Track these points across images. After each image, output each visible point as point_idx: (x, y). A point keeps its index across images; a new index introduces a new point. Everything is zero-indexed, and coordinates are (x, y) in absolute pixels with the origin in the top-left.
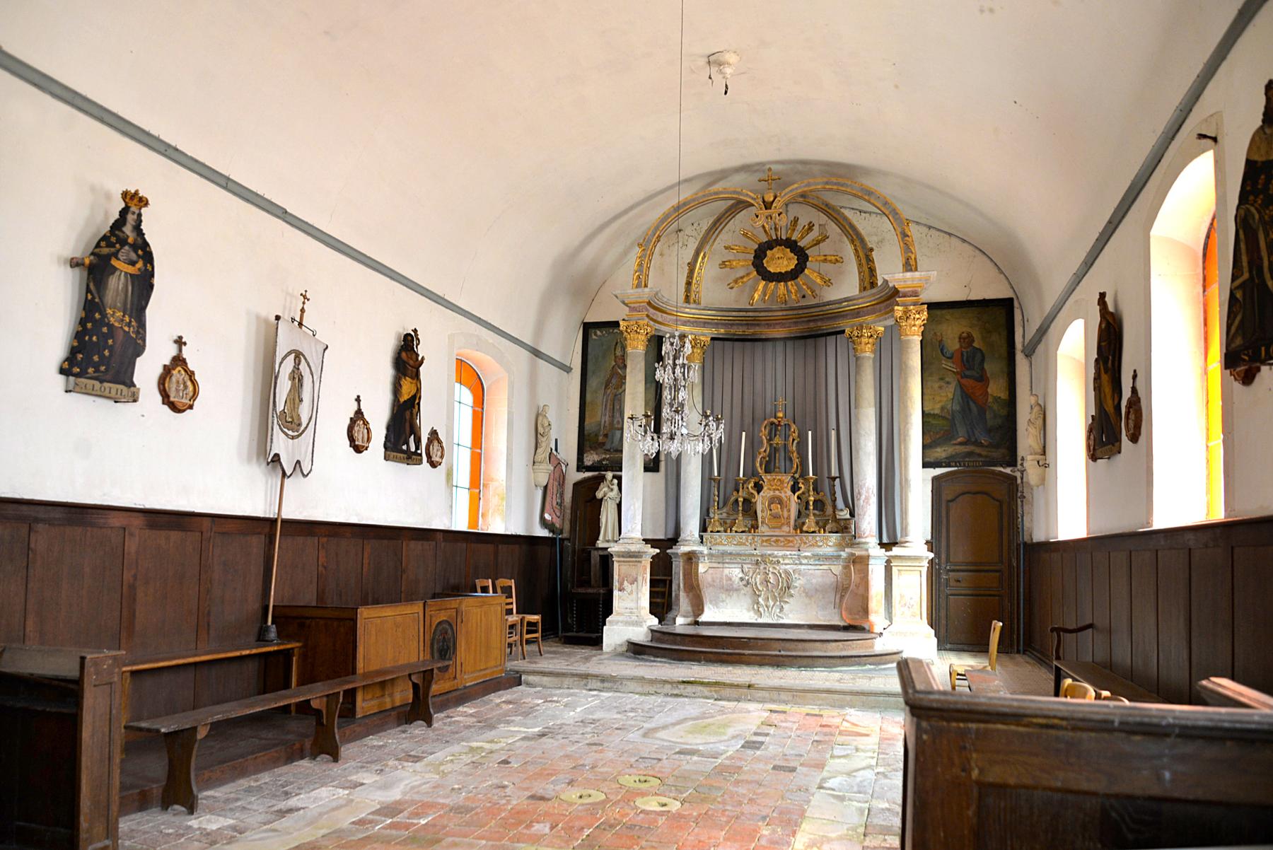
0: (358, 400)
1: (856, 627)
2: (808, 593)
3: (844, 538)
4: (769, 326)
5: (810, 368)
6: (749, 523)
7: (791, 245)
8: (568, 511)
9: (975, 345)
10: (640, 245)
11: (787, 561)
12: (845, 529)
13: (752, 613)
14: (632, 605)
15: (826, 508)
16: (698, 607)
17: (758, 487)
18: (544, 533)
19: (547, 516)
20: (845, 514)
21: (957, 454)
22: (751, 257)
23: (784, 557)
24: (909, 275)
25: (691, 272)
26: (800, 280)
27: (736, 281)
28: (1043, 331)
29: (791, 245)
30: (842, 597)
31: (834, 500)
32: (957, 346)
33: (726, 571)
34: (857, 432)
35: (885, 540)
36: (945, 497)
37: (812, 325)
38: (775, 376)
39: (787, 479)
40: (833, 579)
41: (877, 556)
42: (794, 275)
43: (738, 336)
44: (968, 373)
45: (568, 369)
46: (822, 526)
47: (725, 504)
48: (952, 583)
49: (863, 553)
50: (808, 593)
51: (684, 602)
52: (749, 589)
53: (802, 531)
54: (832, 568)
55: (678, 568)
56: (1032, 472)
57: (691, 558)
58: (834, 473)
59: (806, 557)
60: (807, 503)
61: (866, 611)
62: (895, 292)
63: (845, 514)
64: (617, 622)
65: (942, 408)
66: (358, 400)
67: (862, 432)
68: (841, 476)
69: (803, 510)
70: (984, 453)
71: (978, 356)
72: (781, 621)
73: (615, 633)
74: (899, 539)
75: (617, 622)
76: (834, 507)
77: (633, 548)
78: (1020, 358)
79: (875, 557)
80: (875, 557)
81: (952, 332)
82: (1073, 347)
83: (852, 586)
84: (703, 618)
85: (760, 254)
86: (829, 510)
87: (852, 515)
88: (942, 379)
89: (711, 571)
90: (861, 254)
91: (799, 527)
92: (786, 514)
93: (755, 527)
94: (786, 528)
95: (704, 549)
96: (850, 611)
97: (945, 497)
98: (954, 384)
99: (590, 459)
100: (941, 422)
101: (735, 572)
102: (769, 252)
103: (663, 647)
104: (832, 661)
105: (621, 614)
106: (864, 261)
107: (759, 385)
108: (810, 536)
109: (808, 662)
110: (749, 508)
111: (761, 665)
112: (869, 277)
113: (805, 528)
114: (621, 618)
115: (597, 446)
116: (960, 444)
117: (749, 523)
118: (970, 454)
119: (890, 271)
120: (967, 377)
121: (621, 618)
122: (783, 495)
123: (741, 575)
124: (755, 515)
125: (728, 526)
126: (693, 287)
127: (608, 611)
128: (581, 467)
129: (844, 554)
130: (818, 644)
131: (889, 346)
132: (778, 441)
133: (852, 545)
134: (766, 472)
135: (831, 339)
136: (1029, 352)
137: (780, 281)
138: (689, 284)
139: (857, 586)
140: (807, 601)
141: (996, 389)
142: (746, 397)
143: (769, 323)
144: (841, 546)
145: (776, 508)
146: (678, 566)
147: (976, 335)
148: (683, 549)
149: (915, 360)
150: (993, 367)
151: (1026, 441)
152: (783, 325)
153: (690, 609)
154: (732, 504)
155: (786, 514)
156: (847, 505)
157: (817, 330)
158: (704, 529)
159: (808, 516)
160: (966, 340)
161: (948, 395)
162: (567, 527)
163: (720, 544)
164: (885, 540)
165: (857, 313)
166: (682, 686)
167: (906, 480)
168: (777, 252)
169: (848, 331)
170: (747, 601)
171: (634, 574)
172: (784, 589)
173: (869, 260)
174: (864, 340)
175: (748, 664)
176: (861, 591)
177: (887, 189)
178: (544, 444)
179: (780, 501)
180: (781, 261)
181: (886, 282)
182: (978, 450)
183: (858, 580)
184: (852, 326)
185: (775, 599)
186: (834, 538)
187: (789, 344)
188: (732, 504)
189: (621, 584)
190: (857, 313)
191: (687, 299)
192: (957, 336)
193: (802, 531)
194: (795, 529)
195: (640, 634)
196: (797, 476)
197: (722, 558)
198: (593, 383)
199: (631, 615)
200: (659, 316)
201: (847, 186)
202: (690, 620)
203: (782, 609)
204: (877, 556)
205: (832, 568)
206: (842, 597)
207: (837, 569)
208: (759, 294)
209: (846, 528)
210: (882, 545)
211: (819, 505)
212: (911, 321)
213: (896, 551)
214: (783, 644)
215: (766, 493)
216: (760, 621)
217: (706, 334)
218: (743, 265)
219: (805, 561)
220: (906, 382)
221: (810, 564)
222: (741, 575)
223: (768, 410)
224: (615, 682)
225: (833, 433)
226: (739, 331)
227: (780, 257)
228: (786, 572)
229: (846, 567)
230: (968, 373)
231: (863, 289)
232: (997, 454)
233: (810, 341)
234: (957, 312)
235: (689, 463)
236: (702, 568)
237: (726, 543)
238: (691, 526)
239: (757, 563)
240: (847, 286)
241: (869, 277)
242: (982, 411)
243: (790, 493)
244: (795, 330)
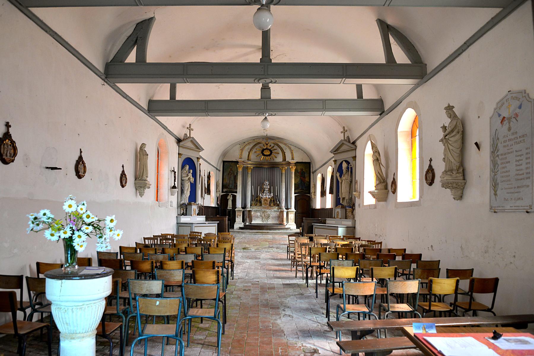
0: (123, 166)
1: (281, 224)
15: (275, 202)
16: (251, 220)
20: (278, 203)
28: (315, 171)
38: (265, 174)
42: (269, 155)
43: (259, 166)
46: (274, 205)
55: (246, 214)
56: (313, 196)
57: (250, 211)
61: (283, 221)
63: (278, 203)
66: (123, 166)
78: (311, 174)
81: (299, 168)
82: (319, 176)
91: (270, 205)
99: (225, 190)
101: (259, 214)
103: (246, 228)
112: (284, 159)
115: (226, 188)
125: (256, 205)
128: (223, 192)
131: (288, 172)
136: (313, 173)
141: (307, 179)
143: (264, 165)
145: (266, 201)
149: (293, 176)
150: (306, 175)
151: (312, 190)
154: (257, 200)
157: (274, 166)
158: (251, 205)
160: (302, 170)
161: (298, 179)
165: (282, 165)
168: (266, 151)
170: (261, 220)
172: (268, 217)
173: (285, 154)
180: (267, 153)
188: (257, 200)
195: (242, 225)
197: (256, 211)
198: (225, 174)
199: (239, 223)
207: (278, 213)
211: (274, 201)
218: (260, 152)
221: (273, 212)
232: (307, 192)
237: (255, 208)
238: (249, 205)
240: (279, 159)
241: (284, 159)
242: (304, 183)
244: (269, 166)
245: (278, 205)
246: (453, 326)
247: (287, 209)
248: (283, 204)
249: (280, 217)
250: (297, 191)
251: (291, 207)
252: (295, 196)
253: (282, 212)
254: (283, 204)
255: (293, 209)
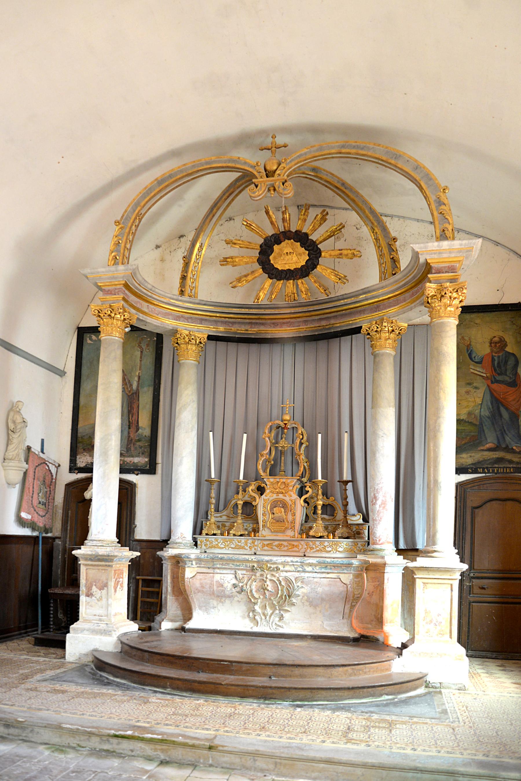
2: (314, 603)
3: (356, 544)
4: (275, 325)
5: (322, 374)
6: (250, 526)
7: (302, 238)
8: (60, 511)
9: (508, 349)
10: (117, 223)
11: (287, 568)
12: (358, 535)
13: (247, 621)
14: (102, 612)
15: (335, 511)
16: (188, 615)
17: (261, 490)
18: (26, 532)
19: (24, 515)
21: (485, 461)
22: (256, 253)
23: (284, 564)
24: (445, 244)
25: (187, 265)
26: (311, 278)
27: (239, 280)
29: (302, 238)
30: (352, 607)
31: (346, 505)
32: (488, 350)
33: (217, 577)
34: (375, 433)
35: (402, 546)
36: (470, 504)
37: (324, 323)
38: (283, 380)
39: (293, 483)
40: (342, 588)
41: (395, 566)
42: (304, 272)
43: (240, 335)
44: (499, 378)
45: (61, 373)
46: (331, 530)
47: (225, 507)
48: (476, 590)
49: (379, 560)
50: (314, 603)
51: (171, 604)
52: (242, 596)
53: (308, 536)
54: (342, 576)
57: (178, 561)
58: (347, 476)
59: (310, 565)
60: (315, 507)
61: (380, 621)
62: (428, 268)
63: (358, 519)
64: (83, 630)
65: (469, 414)
67: (380, 433)
68: (353, 481)
69: (311, 515)
70: (516, 460)
71: (511, 362)
72: (281, 631)
73: (83, 641)
74: (420, 545)
75: (83, 630)
76: (346, 512)
77: (102, 551)
79: (393, 565)
80: (393, 565)
81: (483, 336)
83: (365, 594)
84: (190, 625)
85: (266, 249)
86: (340, 515)
87: (366, 519)
88: (469, 384)
89: (199, 576)
90: (383, 243)
91: (305, 531)
92: (290, 518)
93: (256, 531)
94: (290, 533)
95: (194, 553)
96: (361, 620)
97: (470, 504)
98: (483, 388)
100: (472, 428)
101: (227, 579)
102: (276, 247)
104: (337, 693)
105: (89, 621)
106: (385, 251)
107: (265, 389)
108: (318, 542)
109: (304, 695)
110: (249, 510)
111: (243, 696)
113: (312, 533)
114: (86, 626)
116: (490, 450)
117: (250, 526)
118: (500, 460)
119: (418, 244)
120: (497, 381)
121: (86, 626)
122: (287, 499)
123: (234, 581)
124: (256, 521)
125: (225, 529)
126: (189, 282)
127: (74, 617)
128: (73, 468)
129: (355, 562)
130: (320, 670)
132: (282, 443)
133: (364, 552)
134: (271, 475)
135: (346, 341)
137: (288, 279)
138: (184, 278)
139: (370, 594)
140: (311, 610)
142: (250, 405)
144: (352, 553)
145: (279, 512)
146: (167, 570)
147: (509, 339)
148: (170, 552)
152: (290, 324)
153: (179, 612)
154: (228, 507)
155: (290, 518)
156: (360, 510)
159: (315, 520)
160: (499, 344)
161: (478, 396)
162: (58, 526)
163: (217, 547)
164: (402, 546)
165: (377, 306)
166: (115, 741)
167: (436, 482)
168: (287, 246)
169: (365, 327)
171: (104, 578)
172: (285, 597)
174: (385, 335)
175: (226, 694)
176: (375, 599)
177: (422, 154)
178: (15, 441)
179: (284, 505)
181: (416, 255)
182: (509, 456)
183: (371, 588)
184: (370, 322)
185: (273, 607)
186: (345, 543)
187: (300, 347)
188: (228, 507)
189: (89, 588)
190: (377, 306)
191: (182, 293)
192: (487, 341)
193: (308, 536)
194: (301, 534)
196: (305, 480)
197: (212, 563)
199: (103, 619)
200: (145, 307)
201: (369, 149)
202: (177, 625)
203: (281, 618)
204: (395, 566)
205: (342, 576)
206: (352, 607)
207: (347, 578)
208: (264, 291)
209: (359, 533)
210: (399, 551)
211: (329, 509)
212: (446, 301)
213: (421, 561)
214: (274, 670)
215: (269, 496)
216: (256, 629)
217: (202, 331)
219: (310, 569)
220: (438, 370)
222: (234, 581)
223: (275, 412)
224: (23, 728)
225: (346, 437)
226: (240, 330)
227: (288, 250)
228: (287, 579)
229: (358, 576)
230: (499, 378)
231: (383, 276)
233: (322, 344)
234: (488, 316)
235: (181, 463)
236: (189, 573)
237: (223, 547)
239: (253, 569)
243: (295, 496)
244: (304, 329)
245: (354, 533)
246: (184, 183)
247: (409, 551)
248: (384, 527)
249: (363, 599)
250: (468, 459)
251: (431, 539)
252: (460, 487)
253: (377, 570)
254: (384, 527)
255: (446, 556)
